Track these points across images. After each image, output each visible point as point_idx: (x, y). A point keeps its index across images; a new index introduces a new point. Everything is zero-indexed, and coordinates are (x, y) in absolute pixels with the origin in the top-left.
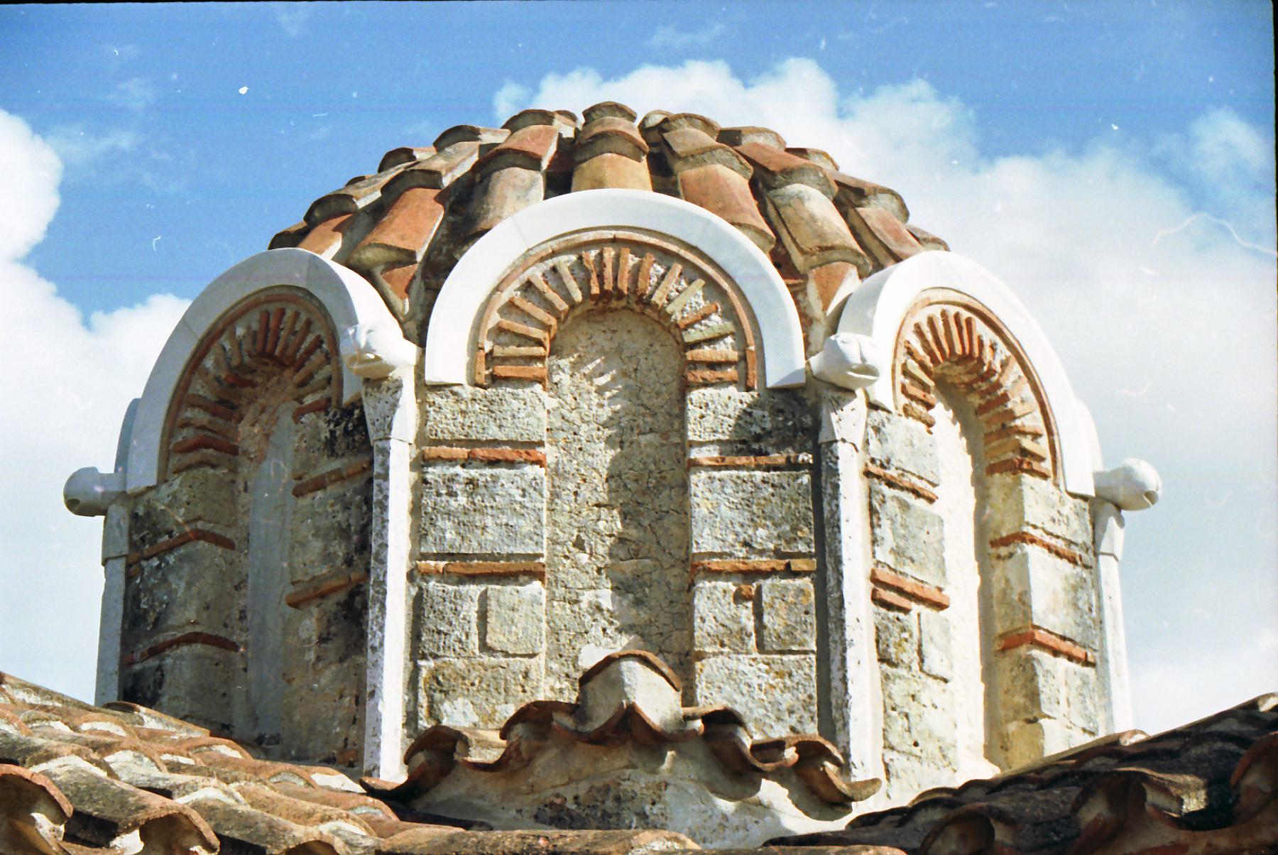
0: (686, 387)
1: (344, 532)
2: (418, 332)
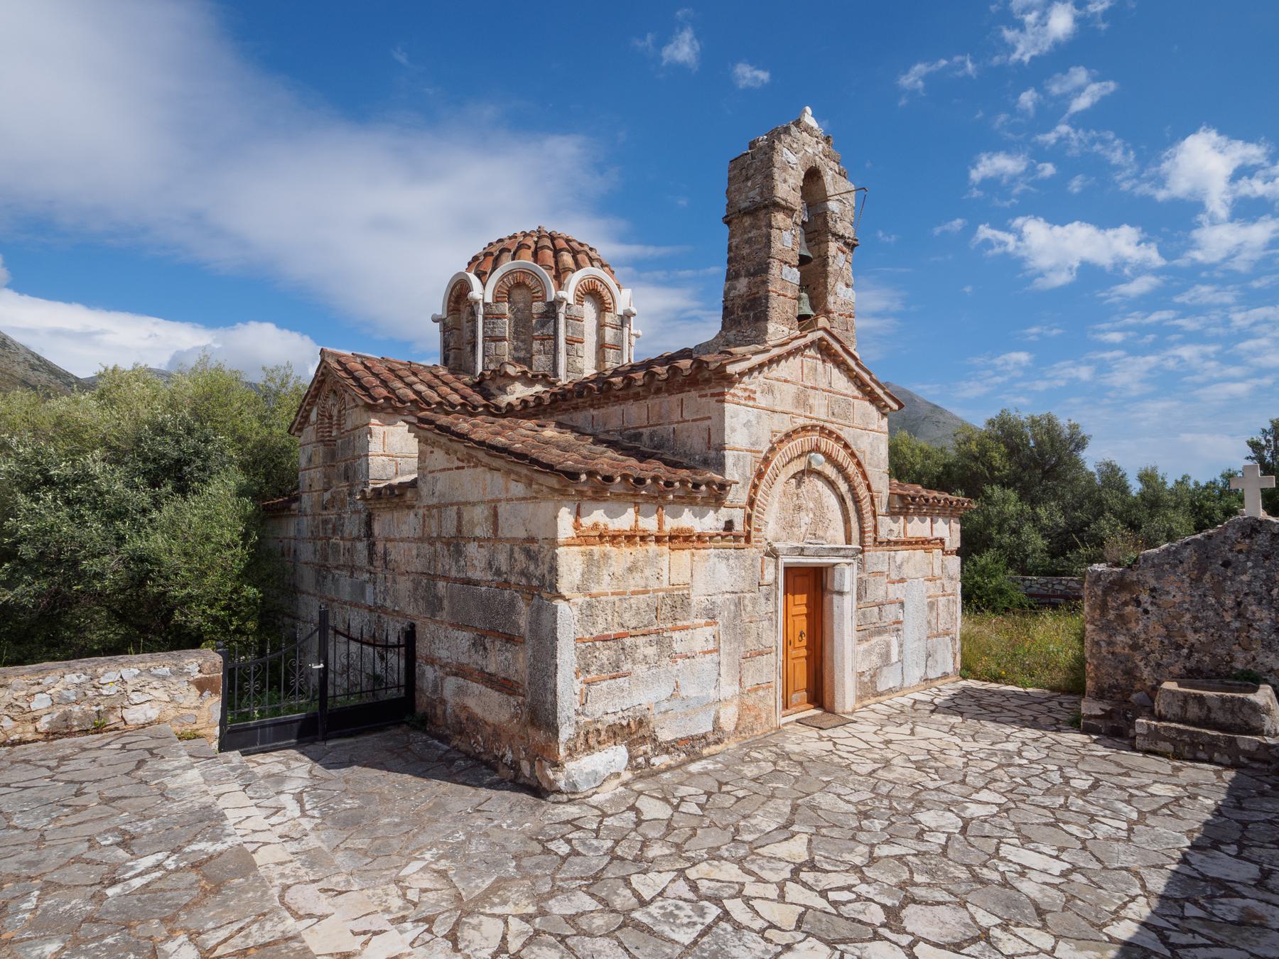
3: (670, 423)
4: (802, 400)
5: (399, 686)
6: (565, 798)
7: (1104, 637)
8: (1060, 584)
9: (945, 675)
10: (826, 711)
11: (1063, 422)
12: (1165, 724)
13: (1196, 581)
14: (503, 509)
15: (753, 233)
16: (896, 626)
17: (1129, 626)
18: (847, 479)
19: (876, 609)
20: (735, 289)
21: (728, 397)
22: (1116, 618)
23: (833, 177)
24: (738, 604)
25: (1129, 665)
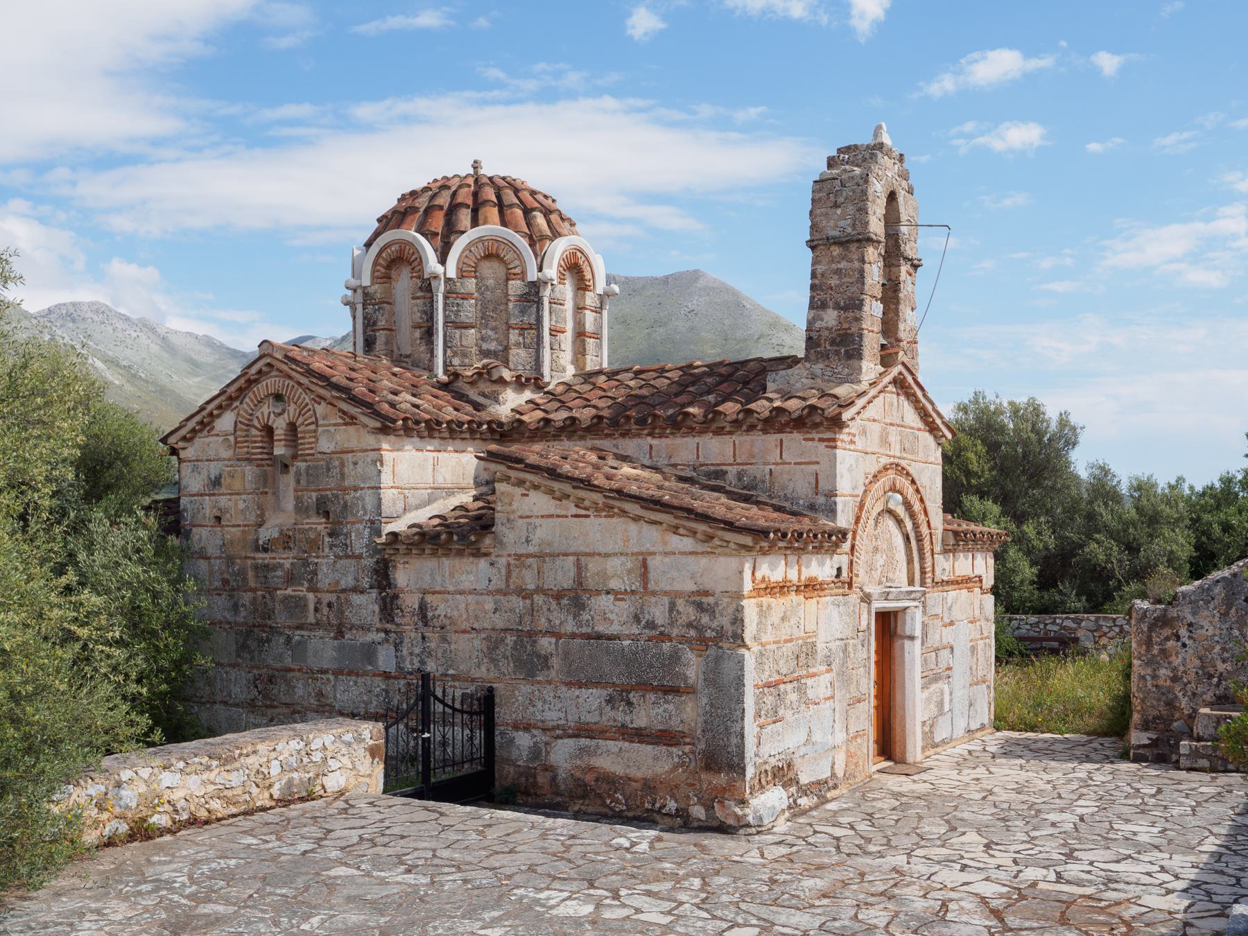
0: (508, 279)
1: (425, 313)
2: (443, 261)
3: (765, 464)
4: (884, 441)
5: (472, 760)
6: (754, 830)
7: (1149, 671)
8: (1054, 623)
9: (983, 727)
10: (896, 762)
11: (1052, 413)
12: (1203, 743)
13: (1224, 615)
14: (653, 562)
15: (843, 265)
16: (947, 672)
17: (1170, 659)
18: (913, 516)
19: (934, 654)
20: (822, 320)
21: (839, 444)
22: (1160, 652)
23: (905, 197)
24: (845, 650)
25: (1170, 696)
